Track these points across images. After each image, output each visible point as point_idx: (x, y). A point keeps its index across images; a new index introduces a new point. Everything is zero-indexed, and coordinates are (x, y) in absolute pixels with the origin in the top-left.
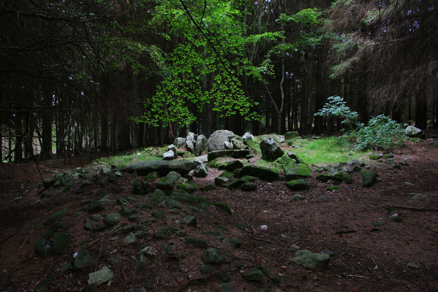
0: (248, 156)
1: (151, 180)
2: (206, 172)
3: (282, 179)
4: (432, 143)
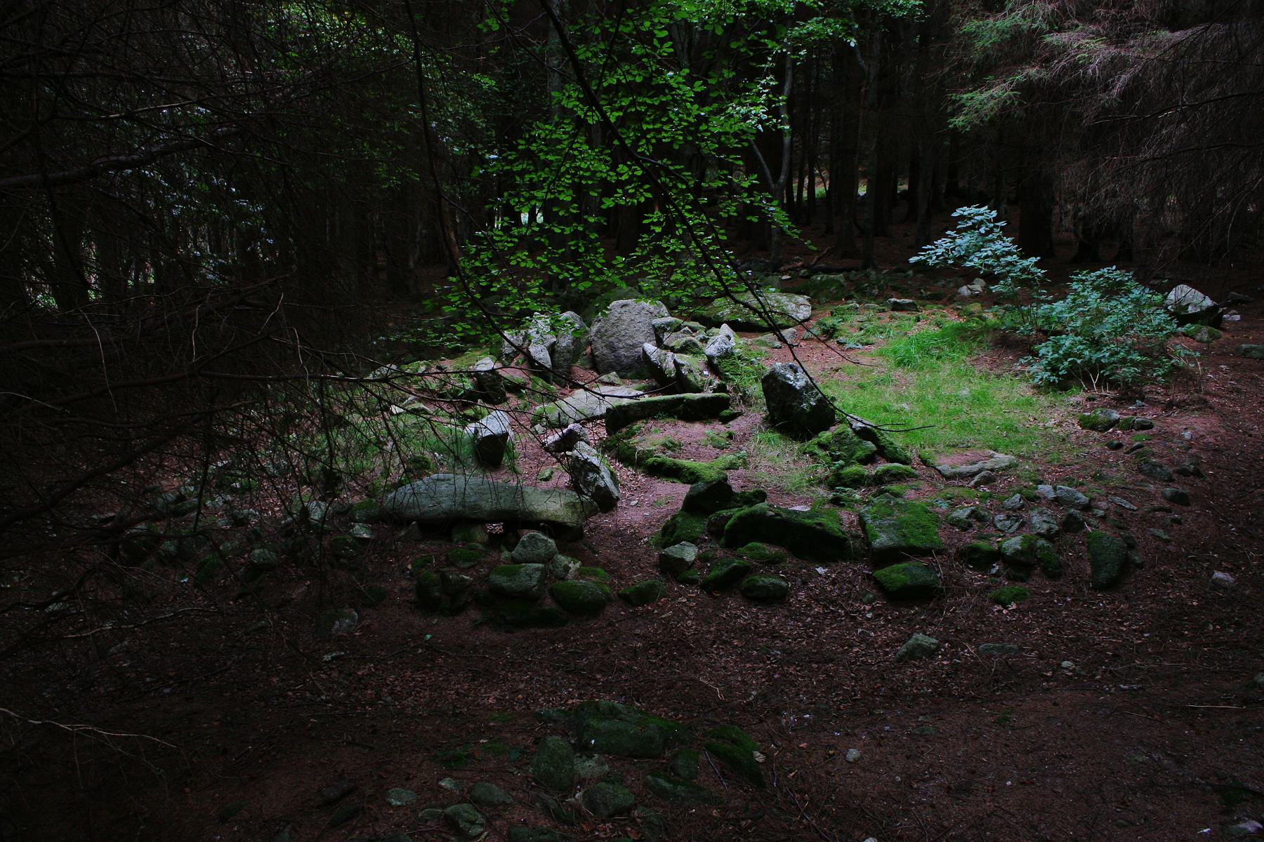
0: (726, 412)
1: (467, 565)
2: (616, 494)
3: (854, 557)
4: (1246, 351)
